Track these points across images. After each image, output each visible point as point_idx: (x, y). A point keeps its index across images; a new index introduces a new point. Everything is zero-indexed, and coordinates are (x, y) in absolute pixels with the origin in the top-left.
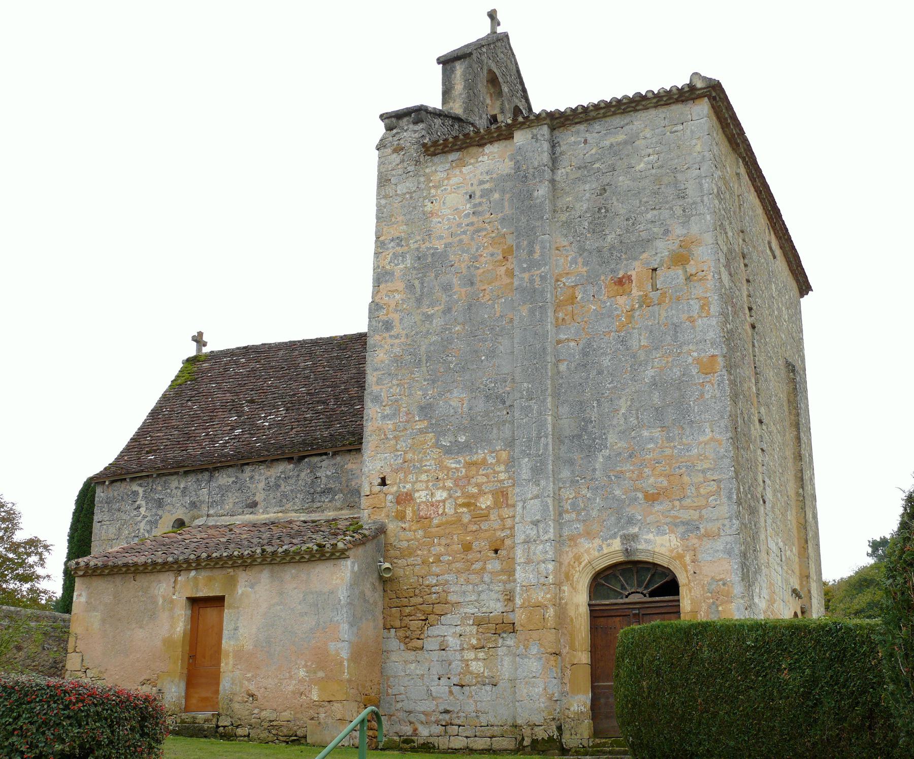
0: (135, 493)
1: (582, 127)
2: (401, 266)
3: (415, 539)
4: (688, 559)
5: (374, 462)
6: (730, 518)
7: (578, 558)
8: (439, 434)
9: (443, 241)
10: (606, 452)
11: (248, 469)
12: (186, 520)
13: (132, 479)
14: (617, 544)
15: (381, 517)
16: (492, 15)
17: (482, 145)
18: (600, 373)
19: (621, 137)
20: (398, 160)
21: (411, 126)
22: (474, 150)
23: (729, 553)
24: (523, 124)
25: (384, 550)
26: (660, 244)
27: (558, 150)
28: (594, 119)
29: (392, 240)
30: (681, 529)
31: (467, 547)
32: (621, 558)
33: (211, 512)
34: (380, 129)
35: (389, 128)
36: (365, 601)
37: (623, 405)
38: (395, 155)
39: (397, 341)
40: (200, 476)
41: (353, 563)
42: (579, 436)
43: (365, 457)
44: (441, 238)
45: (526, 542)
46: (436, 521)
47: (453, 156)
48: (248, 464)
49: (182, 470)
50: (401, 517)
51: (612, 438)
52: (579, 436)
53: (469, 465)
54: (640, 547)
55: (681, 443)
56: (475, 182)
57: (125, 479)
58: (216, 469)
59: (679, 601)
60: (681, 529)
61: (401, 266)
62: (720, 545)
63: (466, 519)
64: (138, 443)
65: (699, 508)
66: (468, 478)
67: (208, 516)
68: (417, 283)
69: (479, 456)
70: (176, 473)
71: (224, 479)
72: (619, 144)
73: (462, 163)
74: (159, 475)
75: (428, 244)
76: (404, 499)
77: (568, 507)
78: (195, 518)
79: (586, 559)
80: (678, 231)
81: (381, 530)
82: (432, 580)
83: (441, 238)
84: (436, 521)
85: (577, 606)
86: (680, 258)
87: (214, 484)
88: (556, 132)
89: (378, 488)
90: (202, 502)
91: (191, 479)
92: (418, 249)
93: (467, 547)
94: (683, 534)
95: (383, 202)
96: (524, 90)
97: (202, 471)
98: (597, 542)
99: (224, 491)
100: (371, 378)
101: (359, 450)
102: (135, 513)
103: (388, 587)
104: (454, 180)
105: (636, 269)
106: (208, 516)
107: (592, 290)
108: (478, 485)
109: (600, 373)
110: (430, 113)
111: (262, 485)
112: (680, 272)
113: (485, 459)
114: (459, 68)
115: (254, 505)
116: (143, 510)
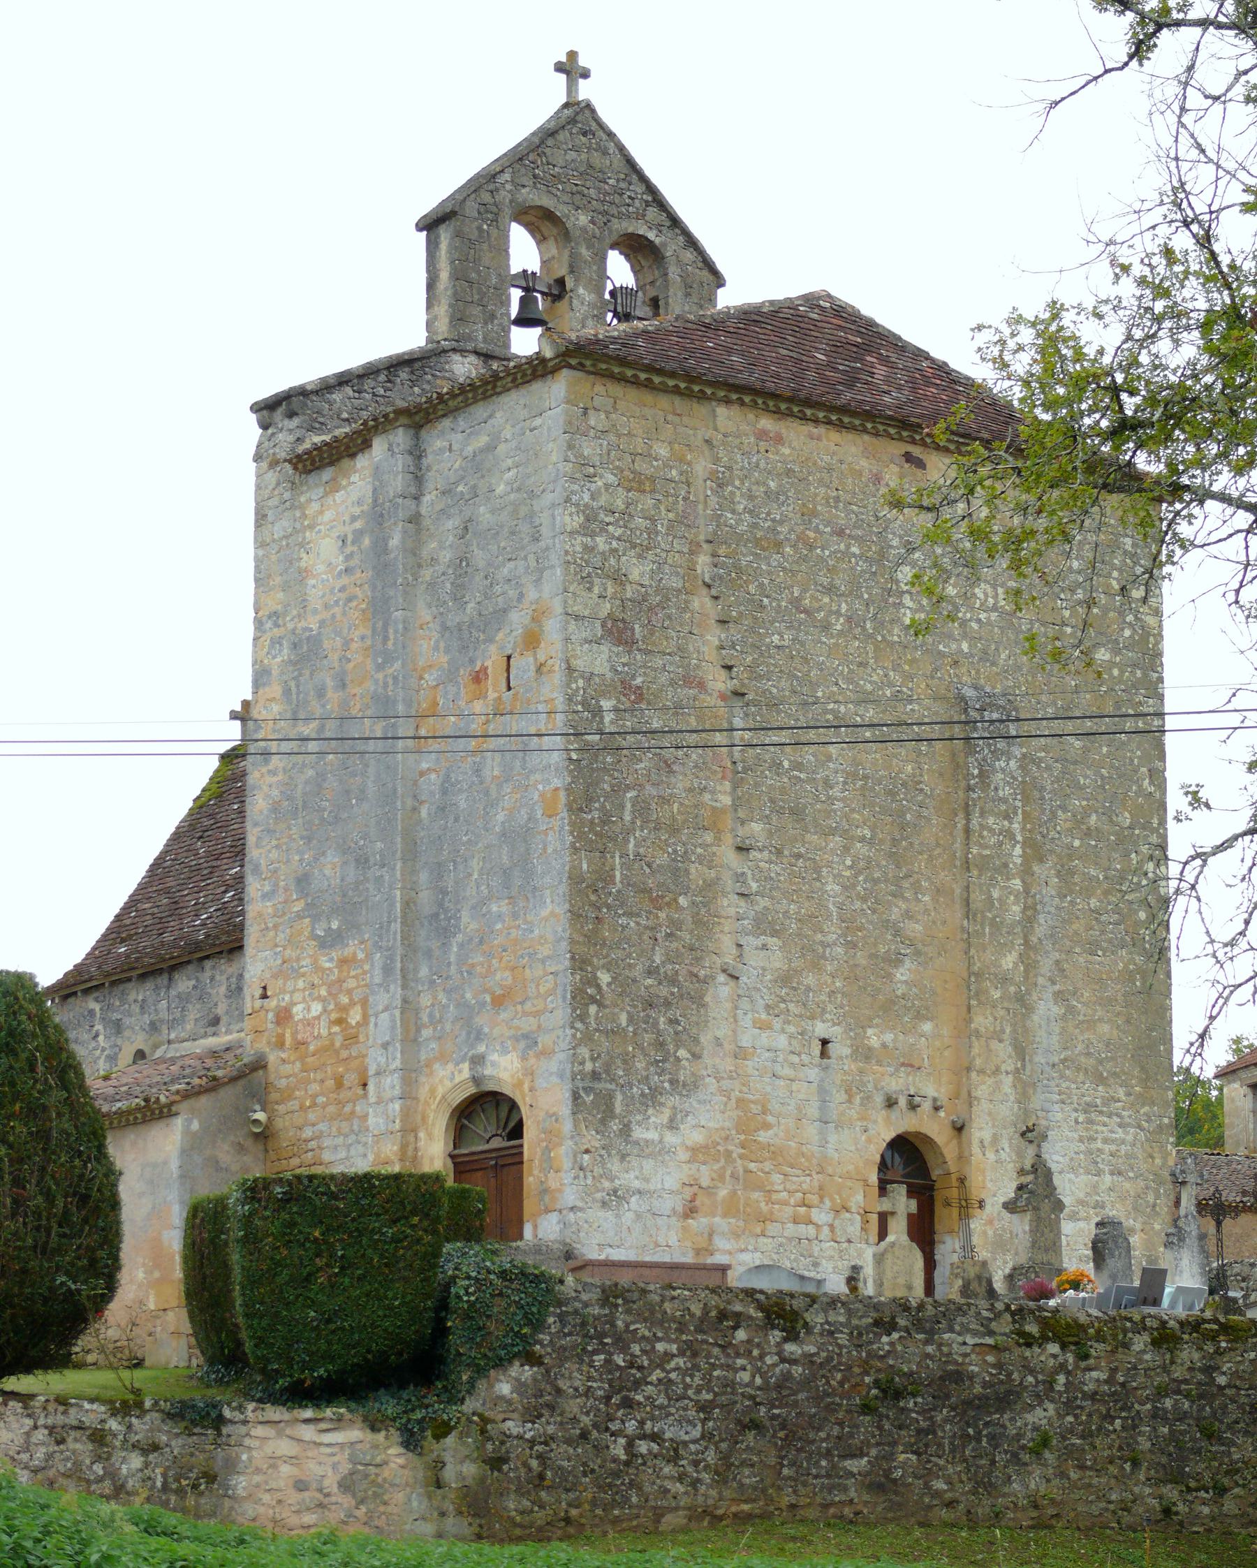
0: (92, 1013)
1: (446, 423)
2: (279, 659)
3: (294, 1075)
4: (526, 1086)
5: (257, 963)
6: (563, 1027)
7: (433, 1092)
8: (316, 918)
9: (318, 617)
10: (460, 937)
11: (208, 964)
12: (147, 1051)
13: (86, 992)
14: (465, 1071)
15: (262, 1045)
16: (571, 69)
17: (353, 456)
18: (456, 820)
19: (483, 440)
20: (274, 481)
21: (286, 422)
22: (346, 463)
23: (561, 1076)
24: (376, 427)
25: (261, 1095)
26: (514, 616)
27: (425, 462)
28: (457, 409)
29: (269, 617)
30: (522, 1044)
31: (339, 1084)
32: (471, 1090)
33: (172, 1036)
34: (251, 431)
35: (264, 426)
36: (218, 1169)
37: (475, 864)
38: (270, 474)
39: (275, 779)
40: (159, 980)
41: (189, 1121)
42: (436, 915)
43: (248, 960)
44: (315, 612)
45: (378, 1074)
46: (312, 1048)
47: (327, 474)
48: (207, 957)
49: (134, 973)
50: (280, 1044)
51: (465, 916)
52: (436, 915)
53: (343, 962)
54: (487, 1072)
55: (526, 922)
56: (347, 518)
57: (75, 993)
58: (173, 968)
59: (521, 1146)
60: (522, 1044)
61: (279, 659)
62: (553, 1065)
63: (338, 1042)
64: (119, 930)
65: (537, 1014)
66: (341, 981)
67: (169, 1042)
68: (293, 684)
69: (348, 952)
70: (129, 980)
71: (184, 983)
72: (481, 451)
73: (333, 487)
74: (113, 983)
75: (303, 624)
76: (284, 1016)
77: (425, 1019)
78: (156, 1047)
79: (440, 1091)
80: (532, 594)
81: (259, 1065)
82: (308, 1133)
83: (315, 612)
84: (312, 1048)
85: (432, 1159)
86: (532, 640)
87: (173, 993)
88: (423, 433)
89: (258, 1003)
90: (162, 1021)
91: (149, 984)
92: (293, 631)
93: (339, 1084)
94: (524, 1051)
95: (261, 553)
96: (651, 189)
97: (160, 971)
98: (450, 1066)
99: (184, 999)
100: (251, 839)
101: (241, 947)
102: (93, 1044)
103: (270, 1144)
104: (328, 516)
105: (492, 659)
106: (169, 1042)
107: (452, 689)
108: (349, 992)
109: (456, 820)
110: (316, 392)
111: (223, 990)
112: (531, 659)
113: (355, 954)
114: (445, 234)
115: (216, 1021)
116: (101, 1038)
